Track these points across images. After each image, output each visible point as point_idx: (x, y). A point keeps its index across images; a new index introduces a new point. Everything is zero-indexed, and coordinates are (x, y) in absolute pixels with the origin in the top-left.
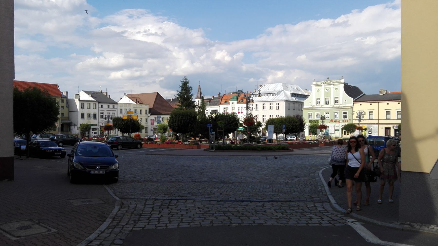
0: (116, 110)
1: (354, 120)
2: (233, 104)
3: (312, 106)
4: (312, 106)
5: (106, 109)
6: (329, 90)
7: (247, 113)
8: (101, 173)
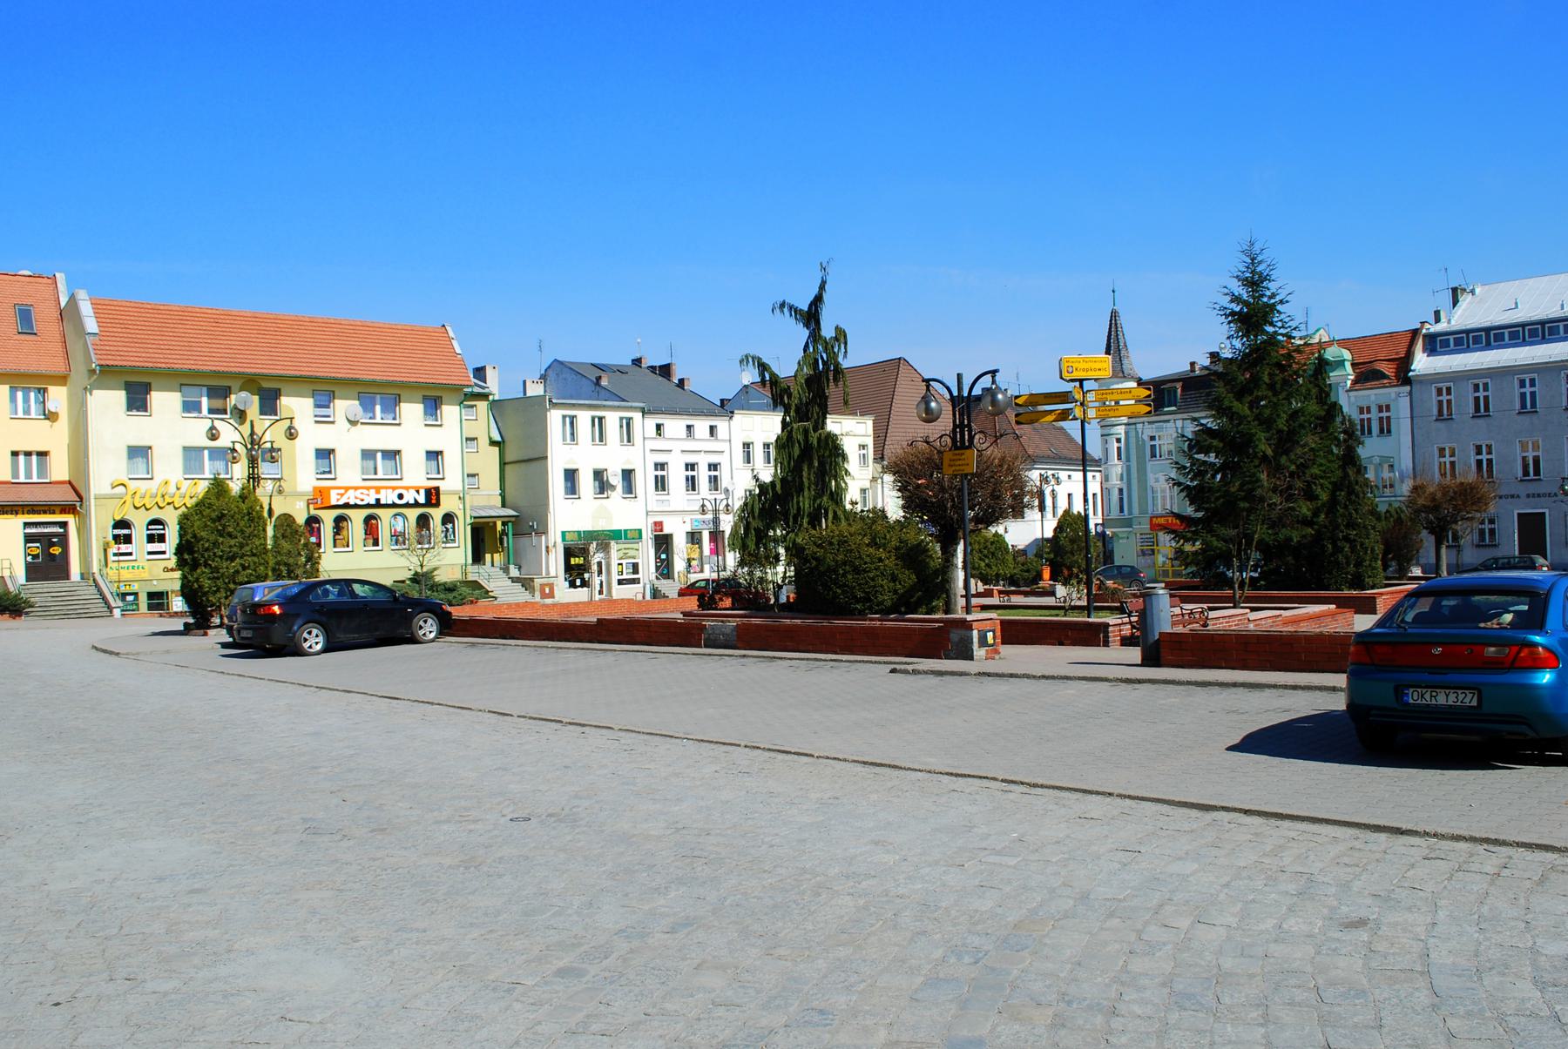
0: (724, 446)
5: (677, 447)
8: (1450, 703)
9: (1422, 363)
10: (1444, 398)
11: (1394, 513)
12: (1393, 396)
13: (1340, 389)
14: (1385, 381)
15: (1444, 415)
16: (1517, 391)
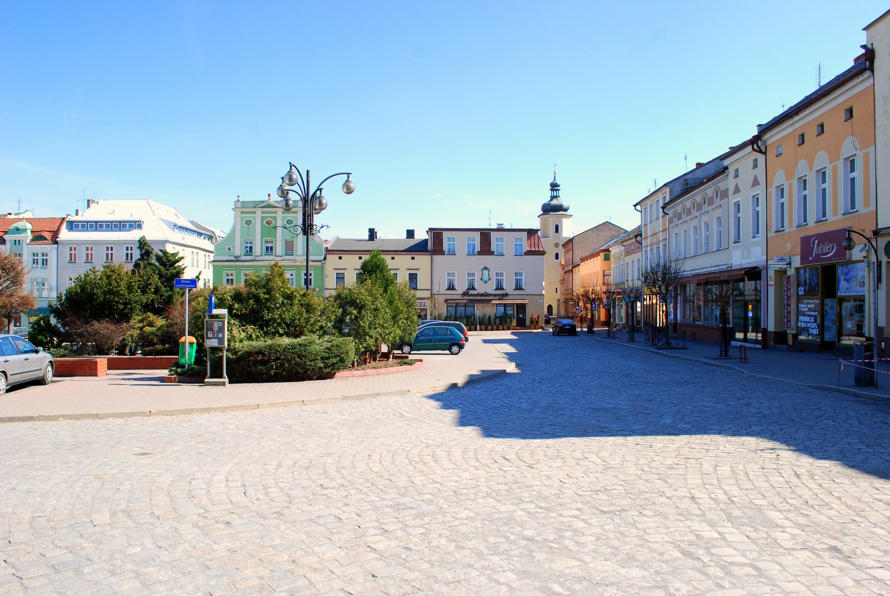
1: (429, 290)
2: (15, 244)
3: (235, 257)
4: (235, 257)
6: (264, 222)
7: (839, 311)
9: (65, 235)
10: (90, 252)
11: (9, 306)
12: (49, 249)
13: (24, 243)
14: (46, 241)
15: (72, 260)
16: (105, 252)
